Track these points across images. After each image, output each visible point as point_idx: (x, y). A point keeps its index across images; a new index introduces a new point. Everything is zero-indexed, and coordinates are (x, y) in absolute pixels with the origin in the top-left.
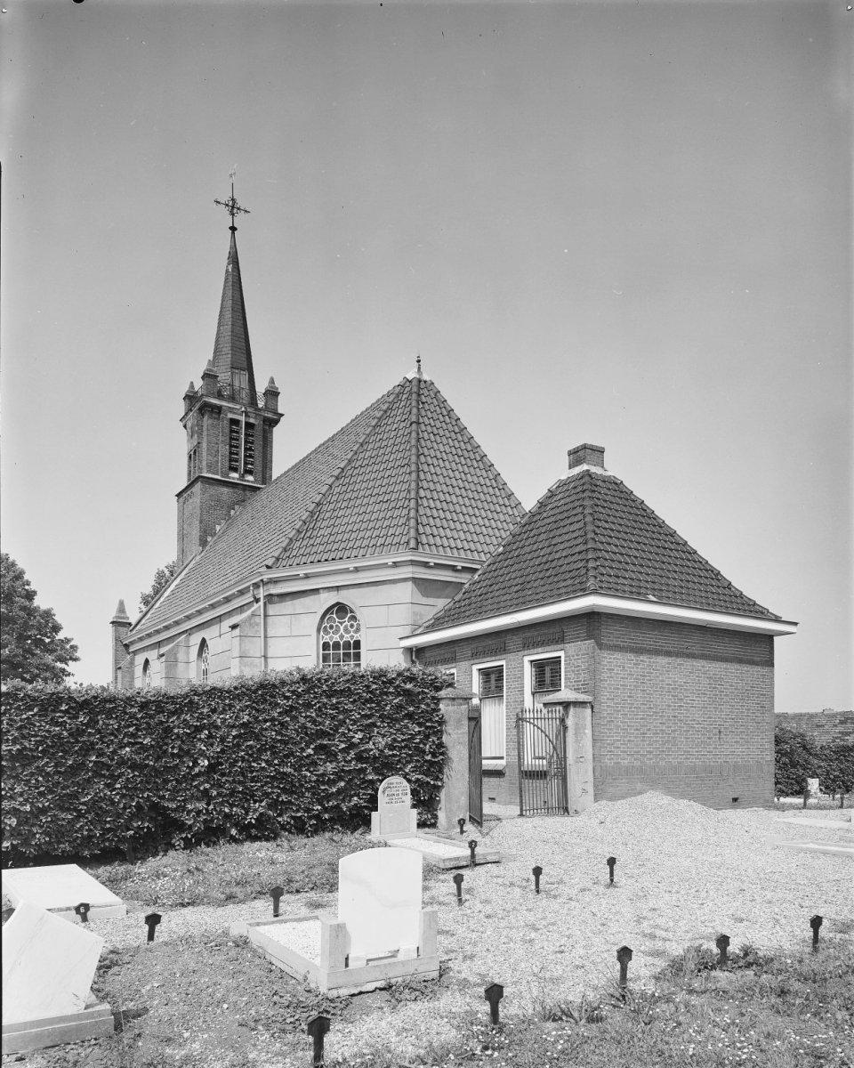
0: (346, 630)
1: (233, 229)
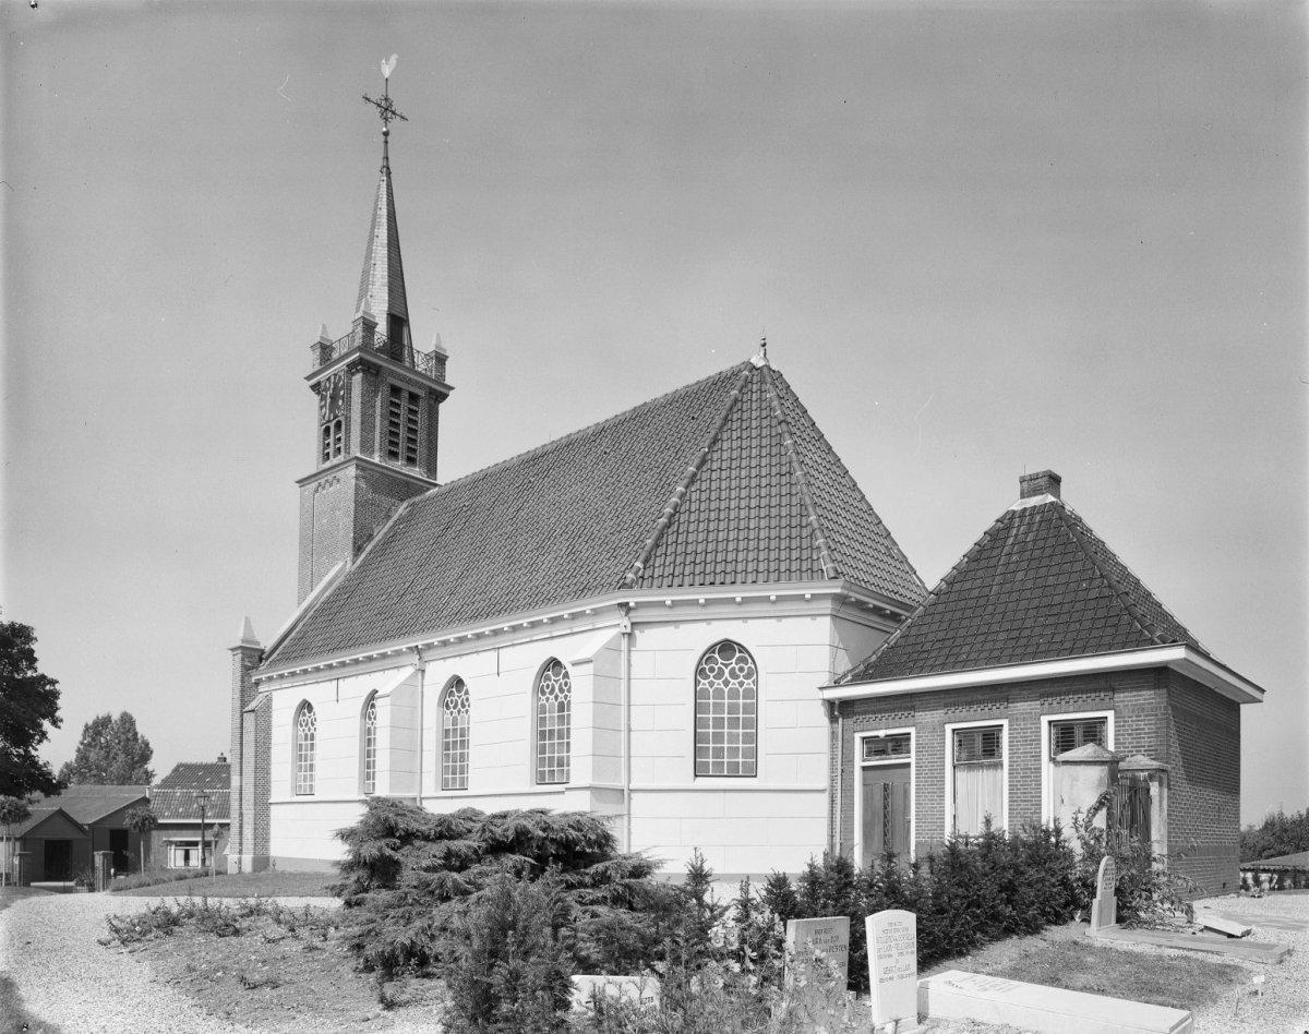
0: (733, 674)
1: (386, 134)
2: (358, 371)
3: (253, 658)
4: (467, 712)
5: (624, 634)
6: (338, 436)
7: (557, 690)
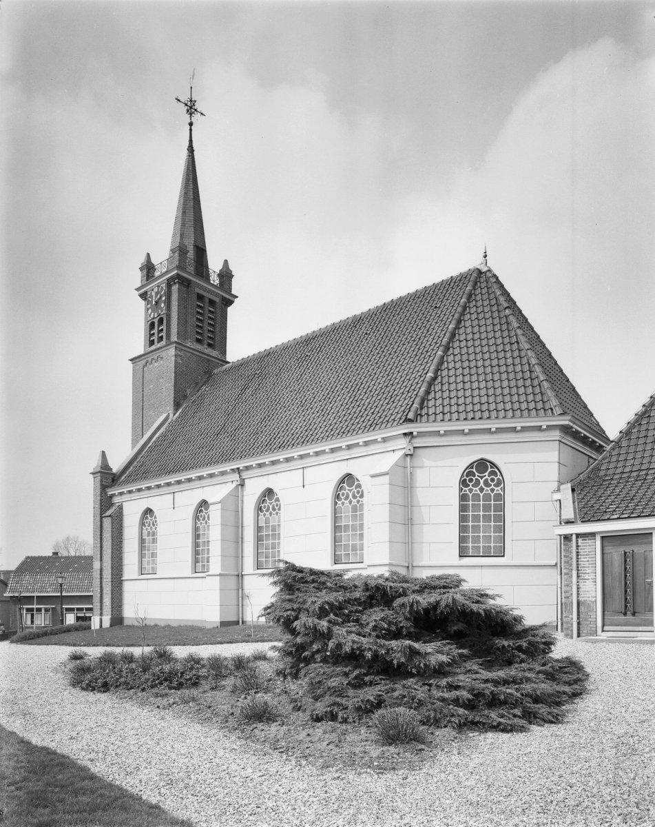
0: (486, 483)
1: (191, 124)
2: (175, 283)
3: (108, 479)
4: (277, 513)
5: (407, 455)
6: (160, 328)
7: (351, 497)
